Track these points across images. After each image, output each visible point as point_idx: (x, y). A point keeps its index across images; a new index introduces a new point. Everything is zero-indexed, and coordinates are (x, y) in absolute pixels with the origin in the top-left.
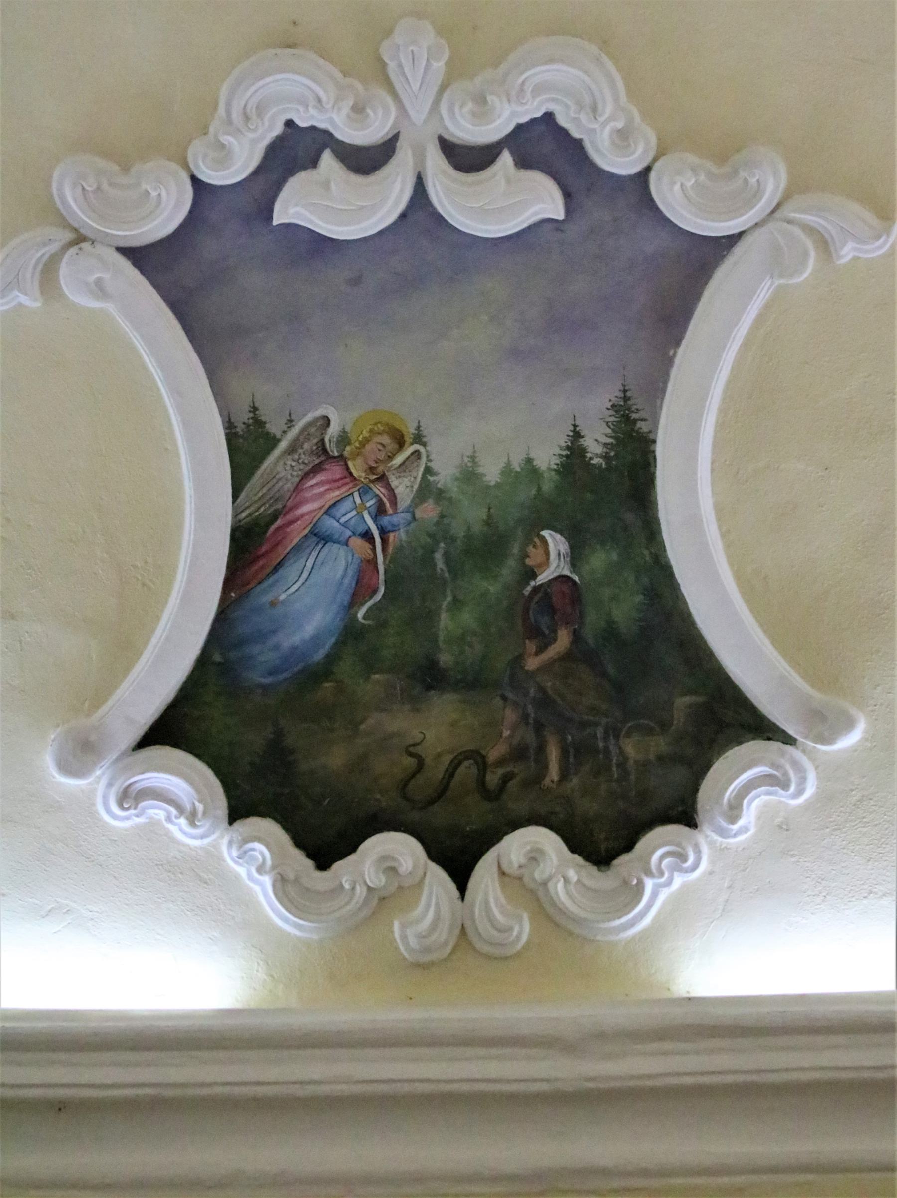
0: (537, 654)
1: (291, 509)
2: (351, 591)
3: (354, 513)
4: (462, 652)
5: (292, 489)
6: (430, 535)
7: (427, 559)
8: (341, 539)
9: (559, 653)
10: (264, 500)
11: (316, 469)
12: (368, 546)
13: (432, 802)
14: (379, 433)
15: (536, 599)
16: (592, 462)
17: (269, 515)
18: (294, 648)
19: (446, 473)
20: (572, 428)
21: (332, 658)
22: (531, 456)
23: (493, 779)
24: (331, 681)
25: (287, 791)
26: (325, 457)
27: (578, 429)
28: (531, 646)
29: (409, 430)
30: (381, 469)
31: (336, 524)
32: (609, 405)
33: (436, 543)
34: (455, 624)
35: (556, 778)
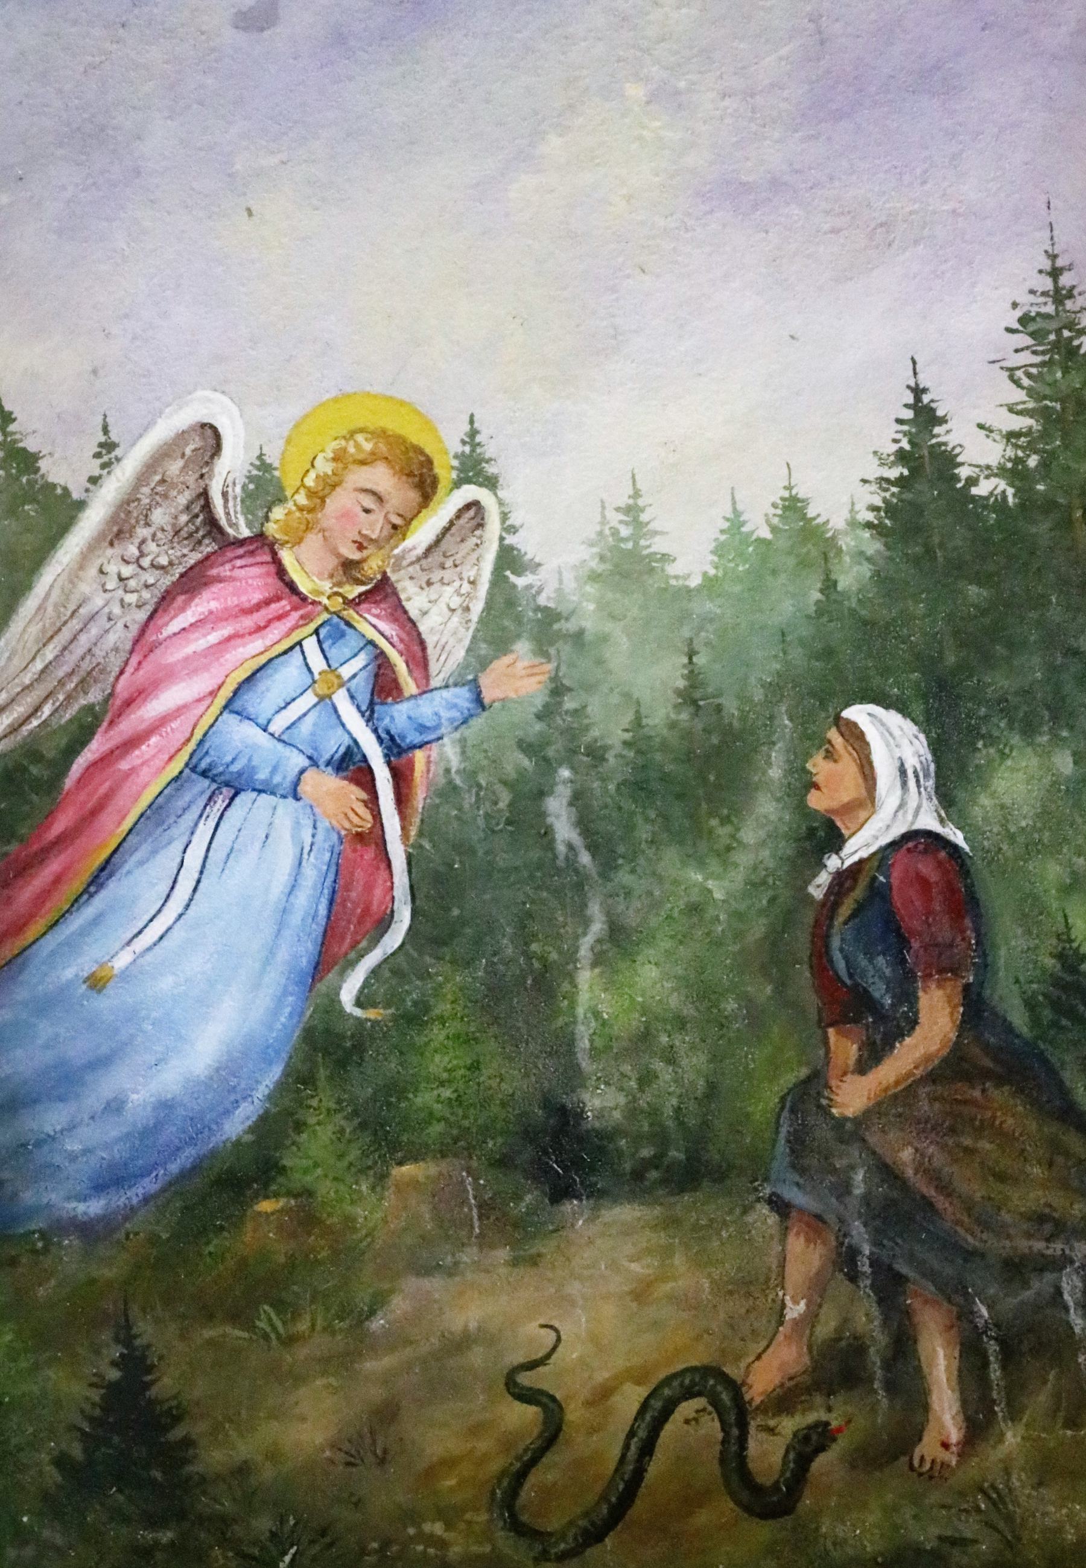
0: (862, 1068)
1: (129, 703)
2: (318, 929)
3: (310, 699)
4: (646, 1079)
5: (128, 646)
6: (526, 747)
7: (530, 796)
8: (277, 779)
9: (928, 1058)
10: (61, 673)
11: (192, 582)
12: (356, 793)
13: (594, 1535)
14: (363, 463)
15: (845, 910)
16: (974, 491)
17: (63, 728)
18: (165, 1106)
19: (561, 564)
20: (910, 399)
21: (277, 1126)
22: (801, 492)
23: (768, 1451)
24: (276, 1195)
25: (167, 1536)
26: (215, 541)
27: (926, 399)
28: (845, 1048)
29: (446, 448)
30: (373, 566)
31: (262, 738)
32: (1012, 319)
33: (547, 766)
34: (623, 1001)
35: (955, 1436)
